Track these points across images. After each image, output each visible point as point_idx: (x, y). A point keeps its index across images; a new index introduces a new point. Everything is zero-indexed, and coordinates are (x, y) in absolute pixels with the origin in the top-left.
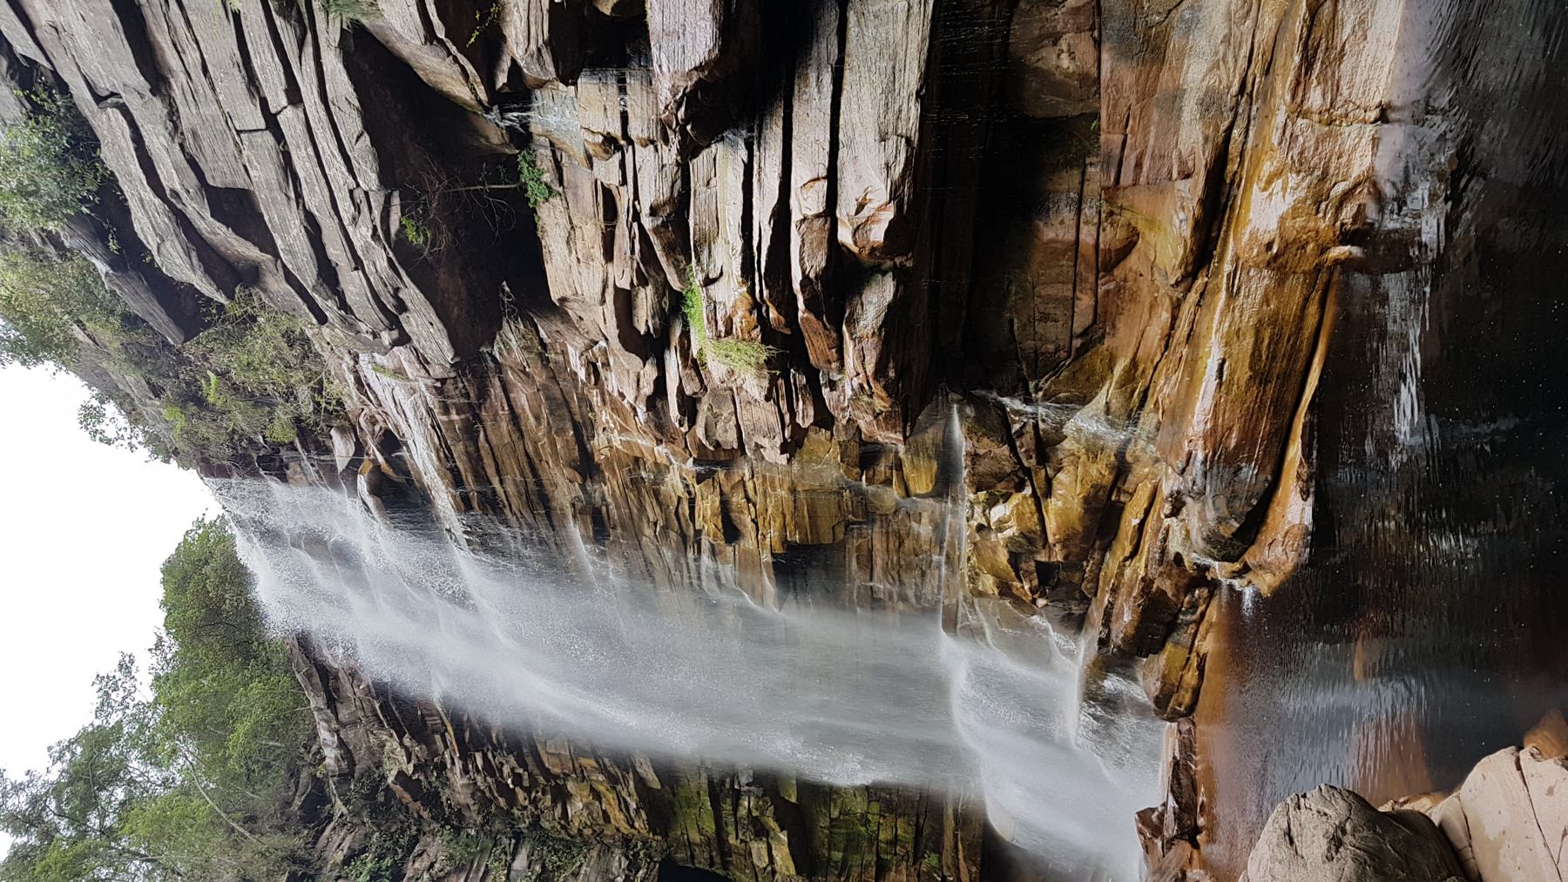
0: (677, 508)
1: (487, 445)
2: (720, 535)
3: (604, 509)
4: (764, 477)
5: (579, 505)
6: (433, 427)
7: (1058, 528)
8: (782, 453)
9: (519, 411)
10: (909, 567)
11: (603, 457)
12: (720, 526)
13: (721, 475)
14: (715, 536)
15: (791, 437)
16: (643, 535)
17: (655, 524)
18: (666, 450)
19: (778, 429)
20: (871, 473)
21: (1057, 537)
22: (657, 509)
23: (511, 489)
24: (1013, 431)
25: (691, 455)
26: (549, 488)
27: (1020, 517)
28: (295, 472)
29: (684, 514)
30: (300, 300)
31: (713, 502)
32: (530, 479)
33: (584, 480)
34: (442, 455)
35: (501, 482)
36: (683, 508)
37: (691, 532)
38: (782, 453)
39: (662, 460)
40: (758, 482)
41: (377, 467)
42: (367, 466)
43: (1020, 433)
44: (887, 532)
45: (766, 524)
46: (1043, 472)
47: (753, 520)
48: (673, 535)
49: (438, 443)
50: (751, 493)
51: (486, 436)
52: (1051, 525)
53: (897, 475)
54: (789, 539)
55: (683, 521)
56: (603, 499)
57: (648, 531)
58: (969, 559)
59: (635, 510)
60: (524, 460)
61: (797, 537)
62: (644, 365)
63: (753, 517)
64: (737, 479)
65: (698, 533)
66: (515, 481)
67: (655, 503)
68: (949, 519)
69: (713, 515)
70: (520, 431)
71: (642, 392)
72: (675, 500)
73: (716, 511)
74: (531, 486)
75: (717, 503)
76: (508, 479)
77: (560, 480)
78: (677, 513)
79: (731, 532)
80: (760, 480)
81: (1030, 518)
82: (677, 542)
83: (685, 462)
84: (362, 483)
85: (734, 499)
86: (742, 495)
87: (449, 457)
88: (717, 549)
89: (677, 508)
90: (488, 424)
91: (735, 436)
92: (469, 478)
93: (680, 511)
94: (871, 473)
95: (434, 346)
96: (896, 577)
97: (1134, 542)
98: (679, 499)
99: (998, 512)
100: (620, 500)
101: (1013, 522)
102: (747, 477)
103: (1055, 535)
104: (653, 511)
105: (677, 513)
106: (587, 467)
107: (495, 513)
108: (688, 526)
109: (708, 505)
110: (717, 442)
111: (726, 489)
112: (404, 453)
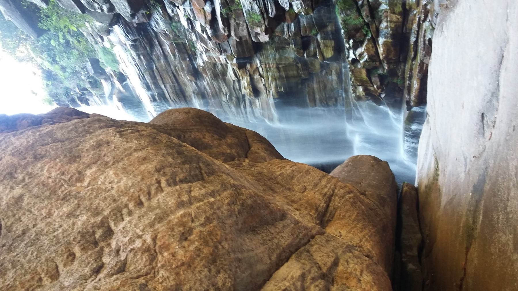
0: (234, 86)
1: (157, 71)
2: (252, 94)
3: (206, 92)
4: (265, 63)
5: (196, 92)
6: (135, 65)
7: (384, 51)
8: (266, 34)
9: (167, 53)
10: (330, 98)
11: (201, 67)
12: (251, 90)
13: (248, 66)
14: (250, 95)
15: (268, 25)
16: (222, 101)
17: (226, 94)
18: (224, 57)
19: (262, 22)
20: (308, 52)
21: (384, 55)
22: (226, 88)
23: (170, 90)
24: (359, 5)
25: (234, 57)
26: (183, 87)
27: (367, 50)
28: (92, 101)
29: (237, 88)
30: (73, 3)
31: (247, 79)
32: (176, 84)
33: (196, 79)
34: (141, 78)
35: (165, 87)
36: (236, 86)
37: (241, 97)
38: (266, 34)
39: (223, 62)
40: (263, 66)
41: (120, 92)
42: (116, 91)
43: (362, 5)
44: (319, 81)
45: (270, 86)
46: (374, 25)
47: (264, 85)
48: (234, 98)
49: (138, 72)
50: (261, 72)
51: (156, 66)
52: (381, 50)
53: (319, 52)
54: (279, 91)
55: (237, 92)
56: (205, 88)
57: (224, 99)
58: (351, 79)
59: (217, 90)
60: (171, 75)
61: (283, 89)
62: (206, 4)
63: (264, 83)
64: (255, 67)
65: (244, 96)
66: (170, 86)
67: (224, 85)
68: (343, 70)
69: (248, 85)
70: (168, 62)
71: (207, 19)
72: (232, 82)
73: (249, 83)
74: (177, 88)
75: (249, 80)
76: (168, 86)
77: (188, 83)
78: (234, 88)
79: (256, 92)
80: (264, 66)
81: (372, 50)
82: (236, 102)
83: (232, 60)
84: (115, 97)
85: (255, 77)
86: (258, 74)
87: (144, 78)
88: (252, 102)
89: (234, 86)
90: (156, 62)
91: (247, 32)
92: (152, 86)
93: (235, 87)
94: (308, 52)
95: (123, 7)
96: (325, 103)
97: (415, 50)
98: (234, 81)
99: (360, 50)
100: (211, 86)
101: (365, 54)
102: (259, 65)
103: (382, 55)
104: (225, 89)
105: (234, 88)
106: (196, 74)
107: (165, 101)
108: (239, 93)
109: (245, 82)
110: (240, 37)
111: (252, 73)
112: (128, 81)
